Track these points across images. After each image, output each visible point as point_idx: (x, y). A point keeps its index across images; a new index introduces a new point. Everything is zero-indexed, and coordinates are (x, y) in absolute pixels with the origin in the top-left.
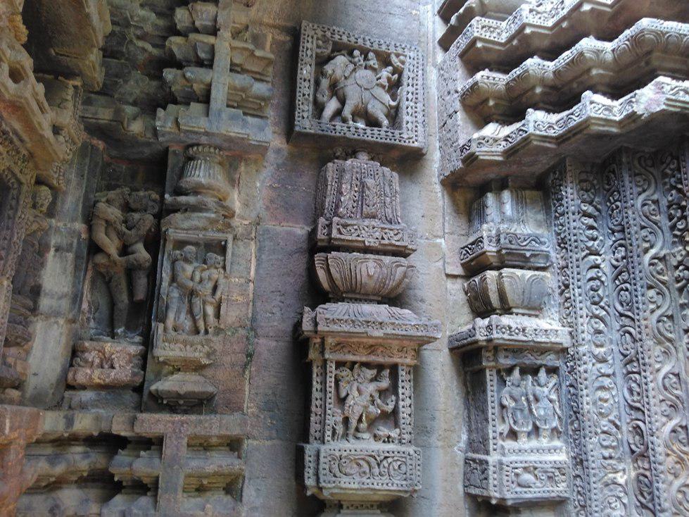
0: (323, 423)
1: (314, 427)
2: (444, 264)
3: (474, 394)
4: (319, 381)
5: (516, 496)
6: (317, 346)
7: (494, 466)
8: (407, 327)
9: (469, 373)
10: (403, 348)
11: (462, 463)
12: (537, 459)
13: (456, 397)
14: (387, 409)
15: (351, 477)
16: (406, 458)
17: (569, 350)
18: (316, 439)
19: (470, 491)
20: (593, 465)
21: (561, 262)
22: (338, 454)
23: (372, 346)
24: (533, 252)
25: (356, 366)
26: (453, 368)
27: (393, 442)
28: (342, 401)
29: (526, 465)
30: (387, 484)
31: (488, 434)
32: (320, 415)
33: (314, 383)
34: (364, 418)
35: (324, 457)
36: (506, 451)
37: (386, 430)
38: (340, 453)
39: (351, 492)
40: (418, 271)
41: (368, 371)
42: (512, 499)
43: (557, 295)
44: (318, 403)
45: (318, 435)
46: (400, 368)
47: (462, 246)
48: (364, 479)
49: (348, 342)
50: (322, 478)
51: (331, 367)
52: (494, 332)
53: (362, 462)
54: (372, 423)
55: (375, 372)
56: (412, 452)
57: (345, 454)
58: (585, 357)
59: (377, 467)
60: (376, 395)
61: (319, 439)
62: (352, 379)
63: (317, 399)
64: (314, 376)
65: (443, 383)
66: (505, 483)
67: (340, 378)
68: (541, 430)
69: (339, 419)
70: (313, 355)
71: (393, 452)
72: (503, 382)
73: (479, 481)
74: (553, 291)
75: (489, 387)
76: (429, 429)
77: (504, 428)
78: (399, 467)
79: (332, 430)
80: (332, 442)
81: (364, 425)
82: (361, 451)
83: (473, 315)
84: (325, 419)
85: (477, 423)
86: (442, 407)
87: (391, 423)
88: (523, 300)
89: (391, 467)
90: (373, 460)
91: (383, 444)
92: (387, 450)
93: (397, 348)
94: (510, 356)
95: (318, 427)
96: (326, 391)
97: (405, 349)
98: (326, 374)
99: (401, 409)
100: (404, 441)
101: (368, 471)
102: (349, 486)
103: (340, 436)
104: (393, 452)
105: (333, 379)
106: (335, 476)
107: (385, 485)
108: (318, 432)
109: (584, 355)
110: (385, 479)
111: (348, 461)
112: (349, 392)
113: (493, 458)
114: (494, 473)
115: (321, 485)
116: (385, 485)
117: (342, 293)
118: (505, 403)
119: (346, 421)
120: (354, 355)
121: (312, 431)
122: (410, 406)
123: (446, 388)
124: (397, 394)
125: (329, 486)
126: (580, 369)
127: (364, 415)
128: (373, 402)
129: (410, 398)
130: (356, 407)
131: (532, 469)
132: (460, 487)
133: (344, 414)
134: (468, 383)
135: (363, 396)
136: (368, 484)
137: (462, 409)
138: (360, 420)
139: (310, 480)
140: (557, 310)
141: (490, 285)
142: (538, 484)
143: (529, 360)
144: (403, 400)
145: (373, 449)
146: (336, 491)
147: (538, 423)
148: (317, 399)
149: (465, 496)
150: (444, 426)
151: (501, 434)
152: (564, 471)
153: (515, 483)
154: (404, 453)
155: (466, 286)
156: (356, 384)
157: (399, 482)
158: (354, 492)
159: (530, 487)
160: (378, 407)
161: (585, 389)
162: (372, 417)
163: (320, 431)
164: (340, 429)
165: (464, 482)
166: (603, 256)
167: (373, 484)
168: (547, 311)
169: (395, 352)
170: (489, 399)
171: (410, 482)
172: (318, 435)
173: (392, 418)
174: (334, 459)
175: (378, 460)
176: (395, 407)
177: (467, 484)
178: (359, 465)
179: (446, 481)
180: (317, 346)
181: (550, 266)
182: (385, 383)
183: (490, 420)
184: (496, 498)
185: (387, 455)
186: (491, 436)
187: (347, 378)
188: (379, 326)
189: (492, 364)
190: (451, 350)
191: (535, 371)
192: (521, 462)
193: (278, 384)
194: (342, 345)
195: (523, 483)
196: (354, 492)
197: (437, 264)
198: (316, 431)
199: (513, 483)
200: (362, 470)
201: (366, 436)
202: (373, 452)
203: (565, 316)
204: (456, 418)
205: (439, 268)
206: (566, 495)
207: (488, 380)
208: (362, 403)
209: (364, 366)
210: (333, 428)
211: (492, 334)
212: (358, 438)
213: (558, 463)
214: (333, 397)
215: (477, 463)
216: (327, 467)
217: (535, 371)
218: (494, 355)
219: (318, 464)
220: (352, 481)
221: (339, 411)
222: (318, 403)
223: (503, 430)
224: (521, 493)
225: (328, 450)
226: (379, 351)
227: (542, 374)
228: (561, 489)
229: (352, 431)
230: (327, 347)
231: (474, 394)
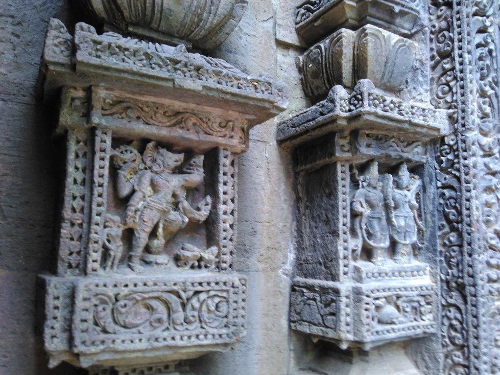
0: (85, 239)
1: (67, 245)
2: (274, 28)
3: (311, 200)
4: (80, 166)
5: (378, 337)
6: (77, 103)
7: (347, 297)
8: (241, 82)
9: (302, 174)
10: (228, 121)
11: (287, 290)
12: (402, 285)
13: (284, 205)
14: (197, 217)
15: (134, 330)
16: (227, 291)
17: (446, 139)
18: (70, 266)
19: (299, 328)
20: (483, 292)
21: (437, 25)
22: (111, 292)
23: (178, 113)
24: (402, 9)
25: (150, 145)
26: (282, 167)
27: (206, 267)
28: (122, 203)
29: (390, 293)
30: (197, 336)
31: (336, 252)
32: (81, 225)
33: (71, 169)
34: (160, 230)
35: (85, 299)
36: (364, 275)
37: (196, 248)
38: (116, 290)
39: (134, 355)
40: (241, 29)
41: (170, 154)
42: (373, 342)
43: (428, 68)
44: (77, 204)
45: (74, 259)
46: (222, 154)
47: (299, 4)
48: (158, 332)
49: (137, 100)
50: (78, 337)
51: (104, 142)
52: (366, 102)
53: (155, 304)
54: (172, 238)
55: (181, 157)
56: (237, 283)
57: (126, 291)
58: (473, 147)
59: (180, 309)
60: (182, 194)
61: (77, 266)
62: (142, 166)
63: (74, 198)
64: (71, 156)
65: (268, 186)
66: (365, 321)
67: (121, 164)
68: (400, 246)
69: (117, 231)
70: (67, 117)
71: (209, 284)
72: (355, 184)
73: (318, 316)
74: (422, 64)
75: (340, 188)
76: (247, 247)
77: (356, 244)
78: (217, 307)
79: (101, 250)
80: (101, 272)
81: (159, 242)
82: (155, 284)
83: (306, 99)
84: (89, 232)
85: (315, 237)
86: (265, 217)
87: (202, 237)
88: (384, 75)
89: (204, 308)
90: (174, 297)
91: (192, 271)
92: (199, 281)
93: (218, 120)
94: (374, 143)
95: (76, 245)
96: (92, 182)
97: (231, 124)
98: (93, 153)
99: (222, 217)
100: (224, 265)
101: (165, 317)
102: (131, 347)
103: (117, 261)
104: (209, 284)
105: (107, 163)
106: (105, 331)
107: (193, 339)
108: (74, 255)
109: (473, 144)
110: (195, 328)
111: (130, 303)
112: (136, 187)
113: (345, 285)
114: (347, 306)
115: (76, 351)
116: (193, 339)
117: (127, 26)
118: (358, 208)
119: (129, 235)
120: (148, 124)
121: (63, 252)
122: (232, 213)
123: (271, 193)
124: (215, 194)
125: (93, 349)
126: (467, 162)
127: (161, 225)
128: (176, 206)
129: (233, 200)
130: (147, 212)
131: (395, 298)
132: (284, 322)
133: (125, 223)
134: (299, 187)
135: (160, 195)
136: (165, 339)
137: (290, 220)
138: (153, 234)
139: (55, 340)
140: (428, 88)
141: (346, 47)
142: (402, 319)
143: (395, 151)
144: (225, 203)
145: (177, 280)
146: (106, 357)
147: (396, 237)
148: (74, 198)
149: (289, 335)
150: (268, 243)
151: (354, 251)
152: (430, 300)
153: (376, 320)
154: (225, 283)
155: (301, 60)
156: (148, 175)
157: (215, 331)
158: (140, 354)
159: (392, 323)
160: (185, 212)
161: (474, 189)
162: (174, 228)
163: (79, 253)
164: (117, 249)
165: (290, 315)
166: (491, 18)
167: (173, 338)
168: (410, 92)
169: (216, 126)
170: (340, 203)
171: (233, 329)
172: (74, 259)
173: (203, 231)
174: (103, 302)
175: (183, 298)
176: (211, 213)
177: (296, 317)
178: (149, 308)
179: (267, 315)
180: (77, 103)
181: (416, 32)
182: (197, 176)
183: (341, 233)
184: (348, 341)
185: (199, 288)
186: (341, 256)
187: (133, 165)
188: (194, 73)
189: (348, 155)
190: (280, 142)
191: (394, 170)
192: (384, 290)
193: (6, 175)
194: (125, 105)
195: (385, 319)
196: (140, 354)
197: (265, 24)
198: (71, 254)
199: (373, 319)
200: (157, 316)
201: (163, 258)
202: (175, 284)
203: (440, 95)
204: (282, 232)
205: (268, 32)
206: (432, 330)
207: (339, 178)
208: (158, 206)
209: (163, 147)
210: (104, 247)
211: (362, 106)
212: (147, 263)
213: (424, 288)
214: (105, 195)
215: (315, 291)
216: (90, 316)
217: (394, 170)
218: (350, 143)
219: (72, 312)
220: (137, 336)
221: (117, 218)
222: (77, 204)
223: (357, 246)
224: (382, 332)
225: (92, 287)
226: (190, 124)
227: (404, 173)
228: (427, 322)
229: (138, 251)
230: (97, 105)
231: (311, 200)
